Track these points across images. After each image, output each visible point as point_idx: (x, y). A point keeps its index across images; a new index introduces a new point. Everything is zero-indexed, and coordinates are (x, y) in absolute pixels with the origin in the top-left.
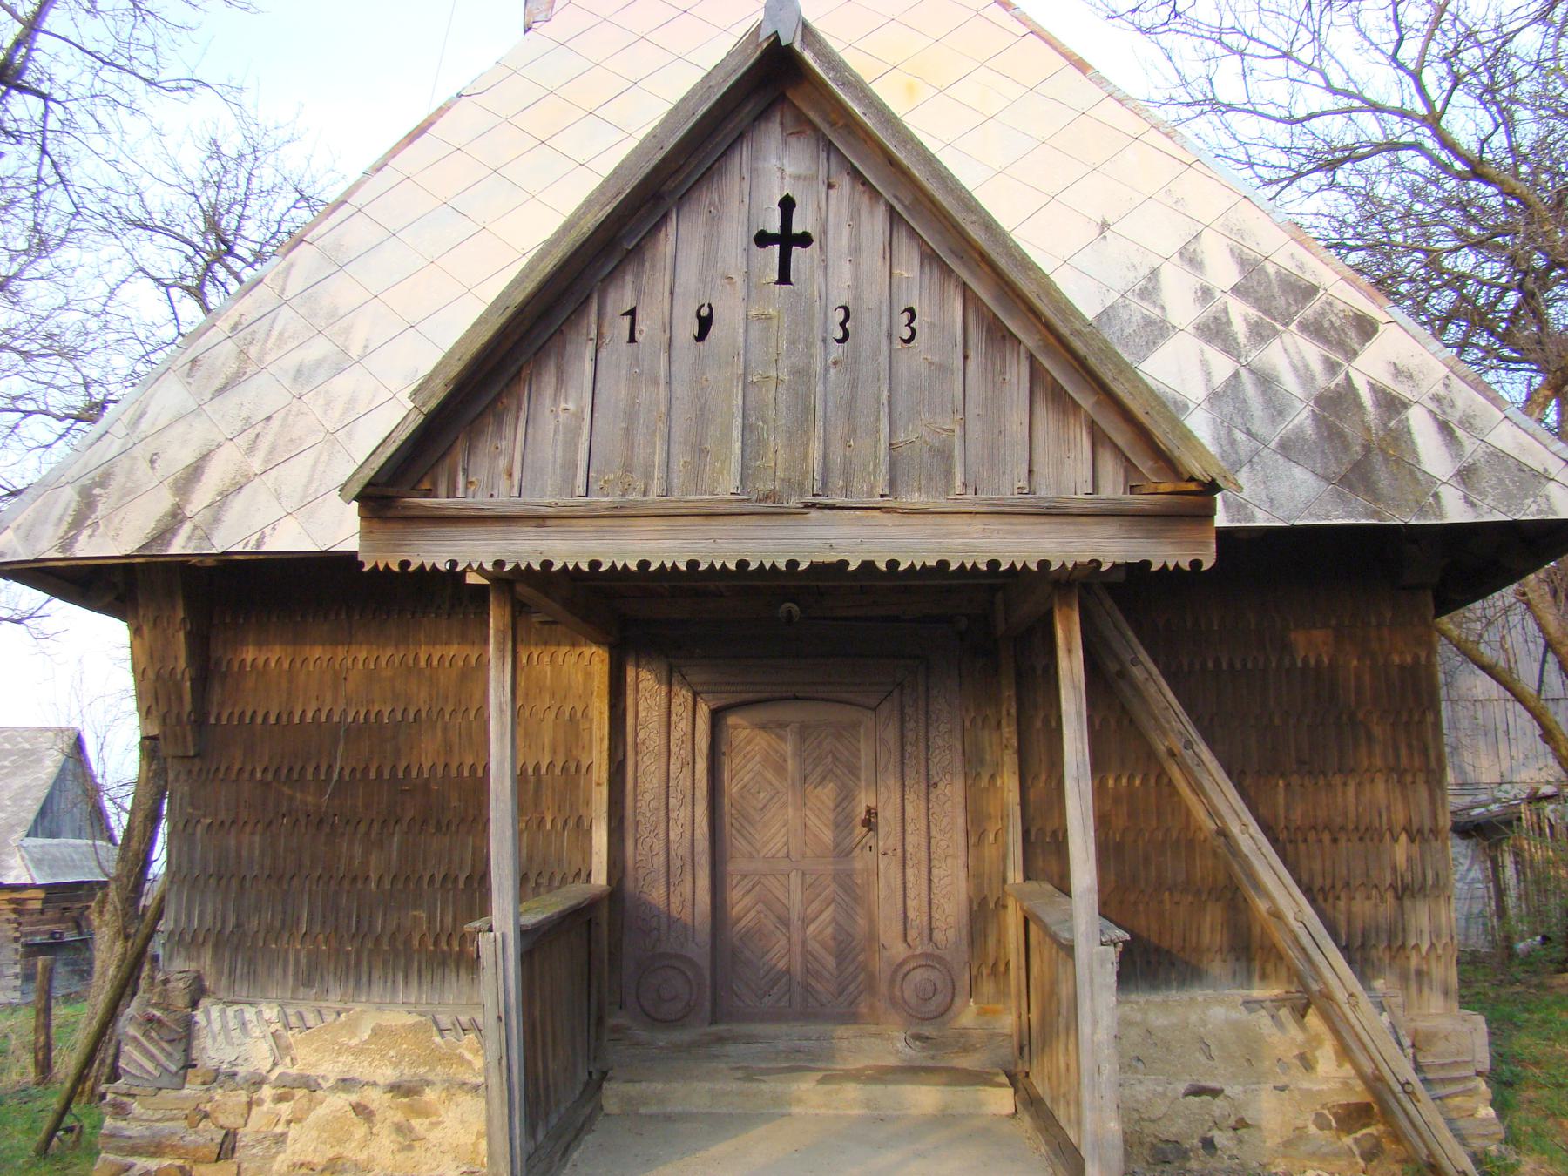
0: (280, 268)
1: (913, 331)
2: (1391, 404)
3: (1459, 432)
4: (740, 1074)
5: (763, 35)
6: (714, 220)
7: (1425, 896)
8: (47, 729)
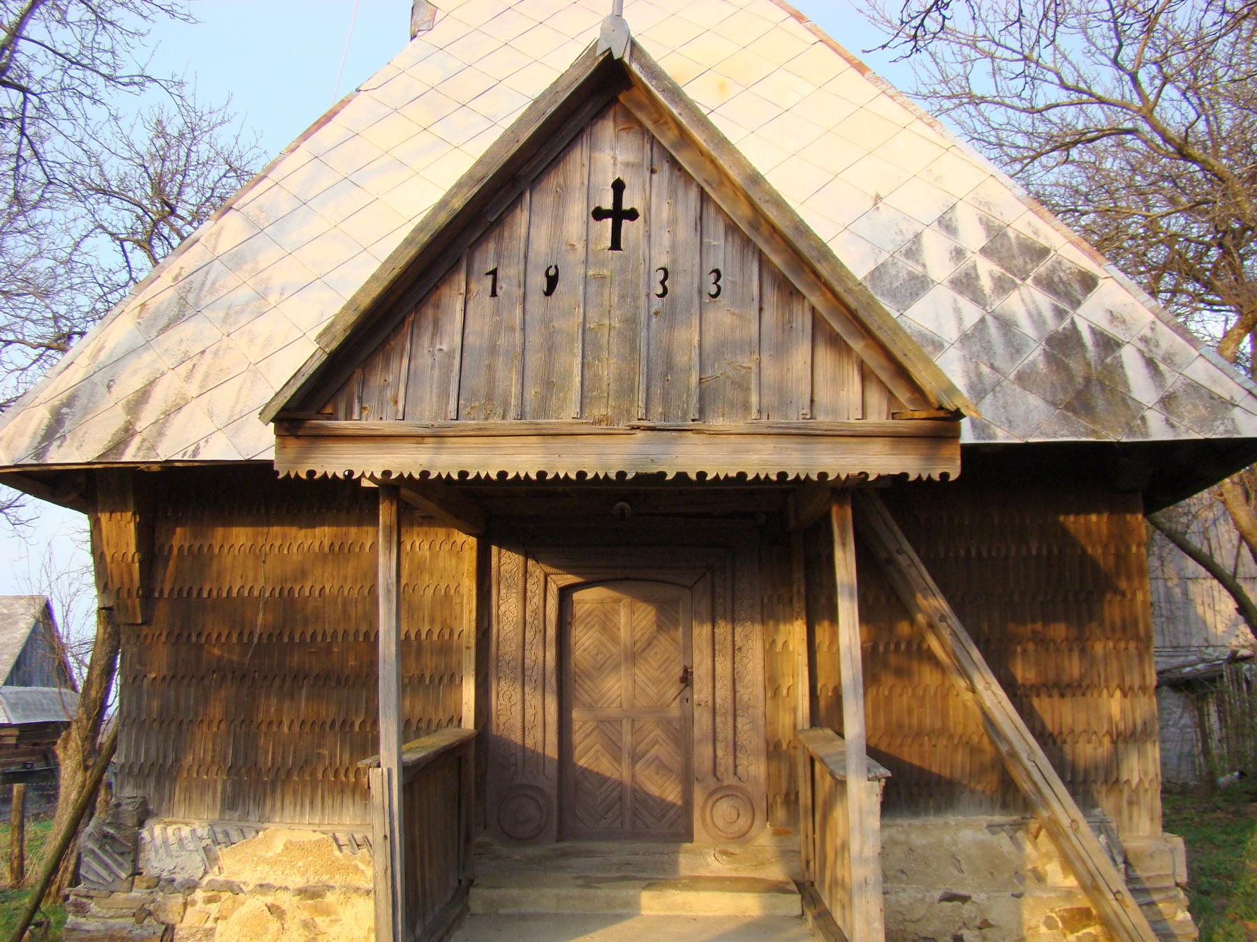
0: (213, 230)
2: (1108, 344)
3: (1162, 367)
4: (580, 882)
5: (599, 52)
6: (562, 198)
7: (1136, 741)
8: (20, 598)
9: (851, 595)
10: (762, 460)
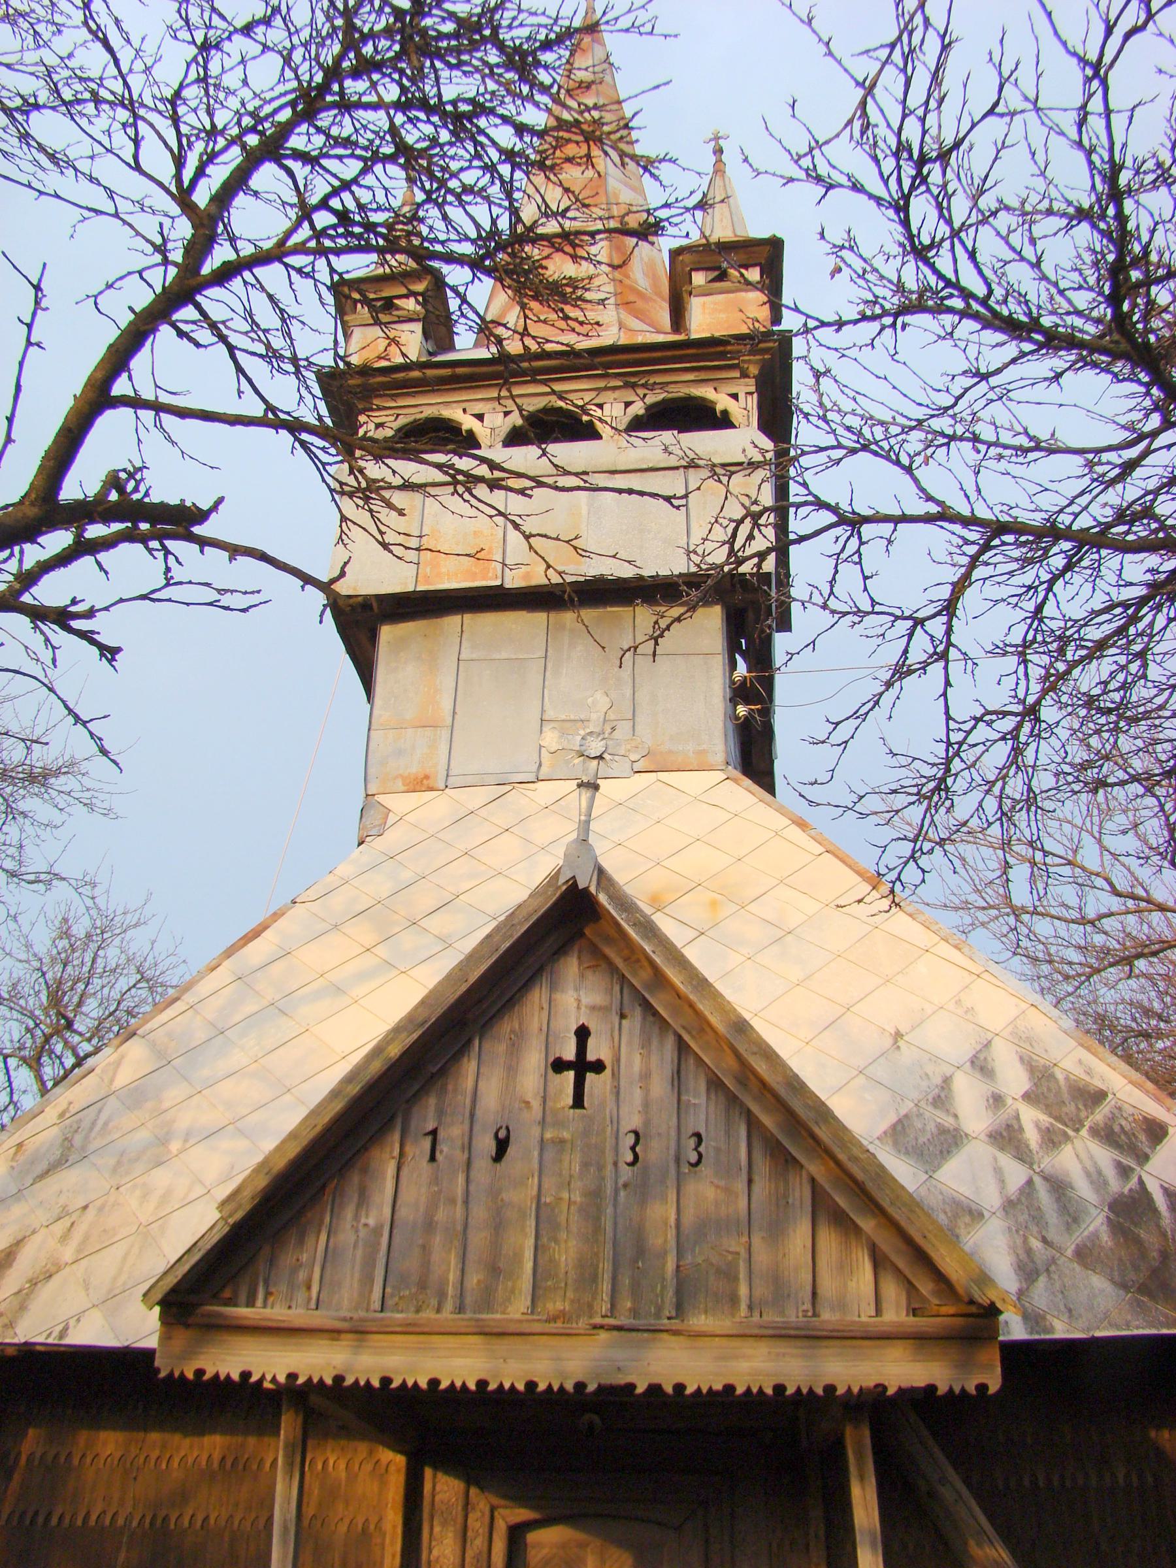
1: (700, 1155)
5: (562, 880)
9: (873, 1545)
10: (755, 1368)
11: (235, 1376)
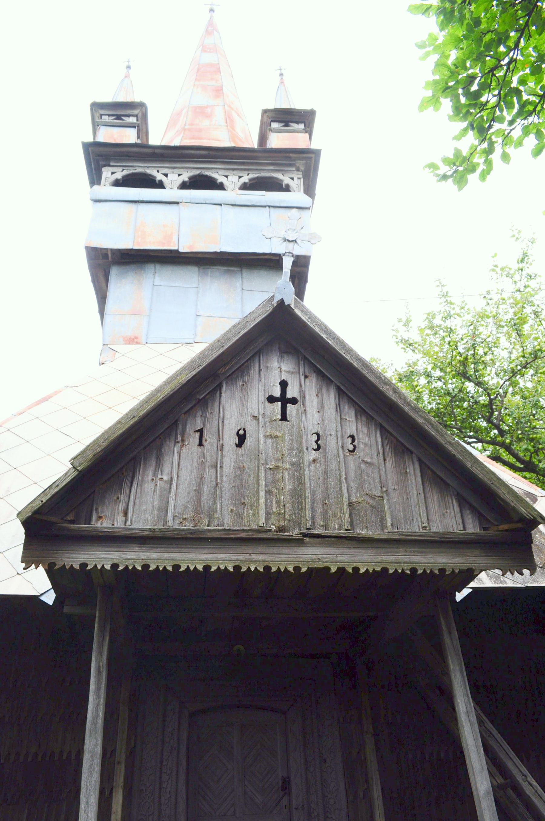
1: (355, 446)
11: (77, 566)
